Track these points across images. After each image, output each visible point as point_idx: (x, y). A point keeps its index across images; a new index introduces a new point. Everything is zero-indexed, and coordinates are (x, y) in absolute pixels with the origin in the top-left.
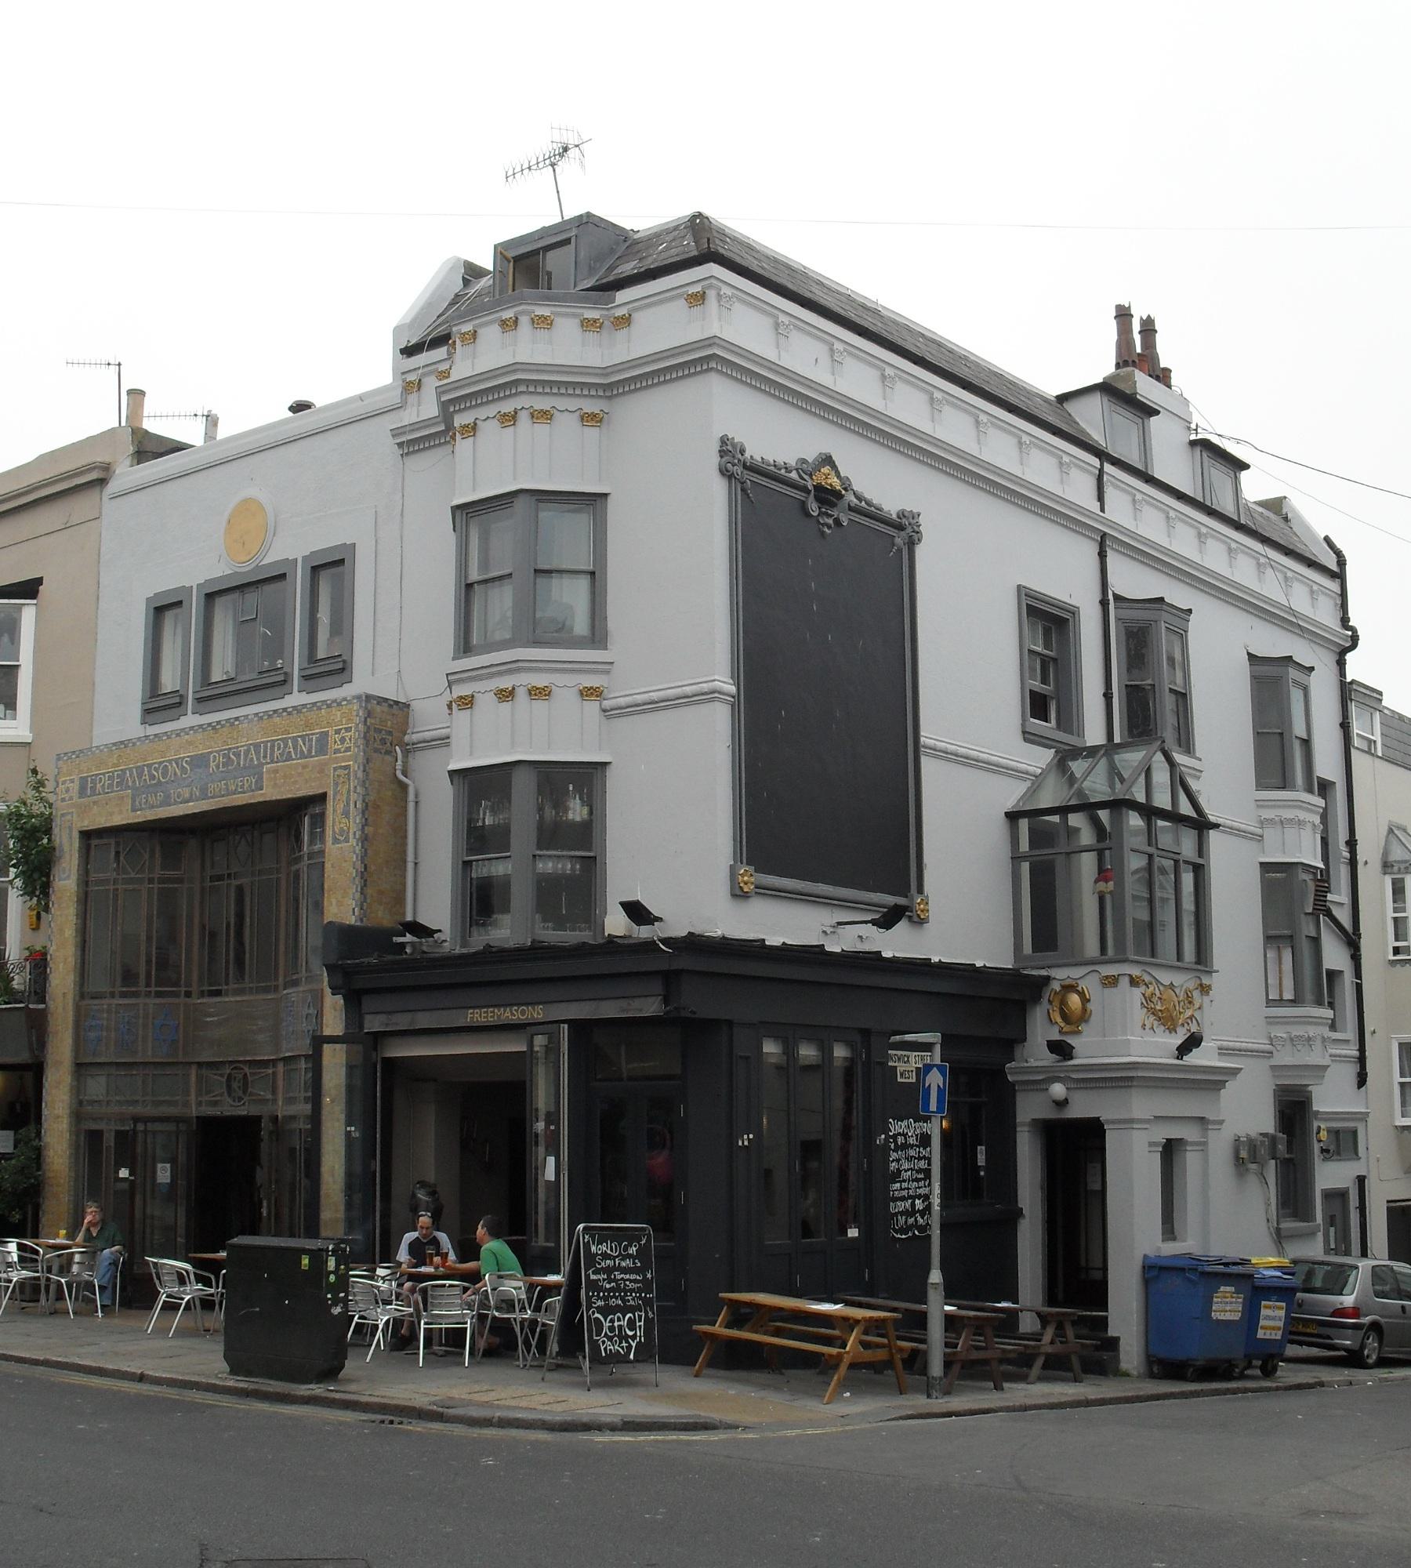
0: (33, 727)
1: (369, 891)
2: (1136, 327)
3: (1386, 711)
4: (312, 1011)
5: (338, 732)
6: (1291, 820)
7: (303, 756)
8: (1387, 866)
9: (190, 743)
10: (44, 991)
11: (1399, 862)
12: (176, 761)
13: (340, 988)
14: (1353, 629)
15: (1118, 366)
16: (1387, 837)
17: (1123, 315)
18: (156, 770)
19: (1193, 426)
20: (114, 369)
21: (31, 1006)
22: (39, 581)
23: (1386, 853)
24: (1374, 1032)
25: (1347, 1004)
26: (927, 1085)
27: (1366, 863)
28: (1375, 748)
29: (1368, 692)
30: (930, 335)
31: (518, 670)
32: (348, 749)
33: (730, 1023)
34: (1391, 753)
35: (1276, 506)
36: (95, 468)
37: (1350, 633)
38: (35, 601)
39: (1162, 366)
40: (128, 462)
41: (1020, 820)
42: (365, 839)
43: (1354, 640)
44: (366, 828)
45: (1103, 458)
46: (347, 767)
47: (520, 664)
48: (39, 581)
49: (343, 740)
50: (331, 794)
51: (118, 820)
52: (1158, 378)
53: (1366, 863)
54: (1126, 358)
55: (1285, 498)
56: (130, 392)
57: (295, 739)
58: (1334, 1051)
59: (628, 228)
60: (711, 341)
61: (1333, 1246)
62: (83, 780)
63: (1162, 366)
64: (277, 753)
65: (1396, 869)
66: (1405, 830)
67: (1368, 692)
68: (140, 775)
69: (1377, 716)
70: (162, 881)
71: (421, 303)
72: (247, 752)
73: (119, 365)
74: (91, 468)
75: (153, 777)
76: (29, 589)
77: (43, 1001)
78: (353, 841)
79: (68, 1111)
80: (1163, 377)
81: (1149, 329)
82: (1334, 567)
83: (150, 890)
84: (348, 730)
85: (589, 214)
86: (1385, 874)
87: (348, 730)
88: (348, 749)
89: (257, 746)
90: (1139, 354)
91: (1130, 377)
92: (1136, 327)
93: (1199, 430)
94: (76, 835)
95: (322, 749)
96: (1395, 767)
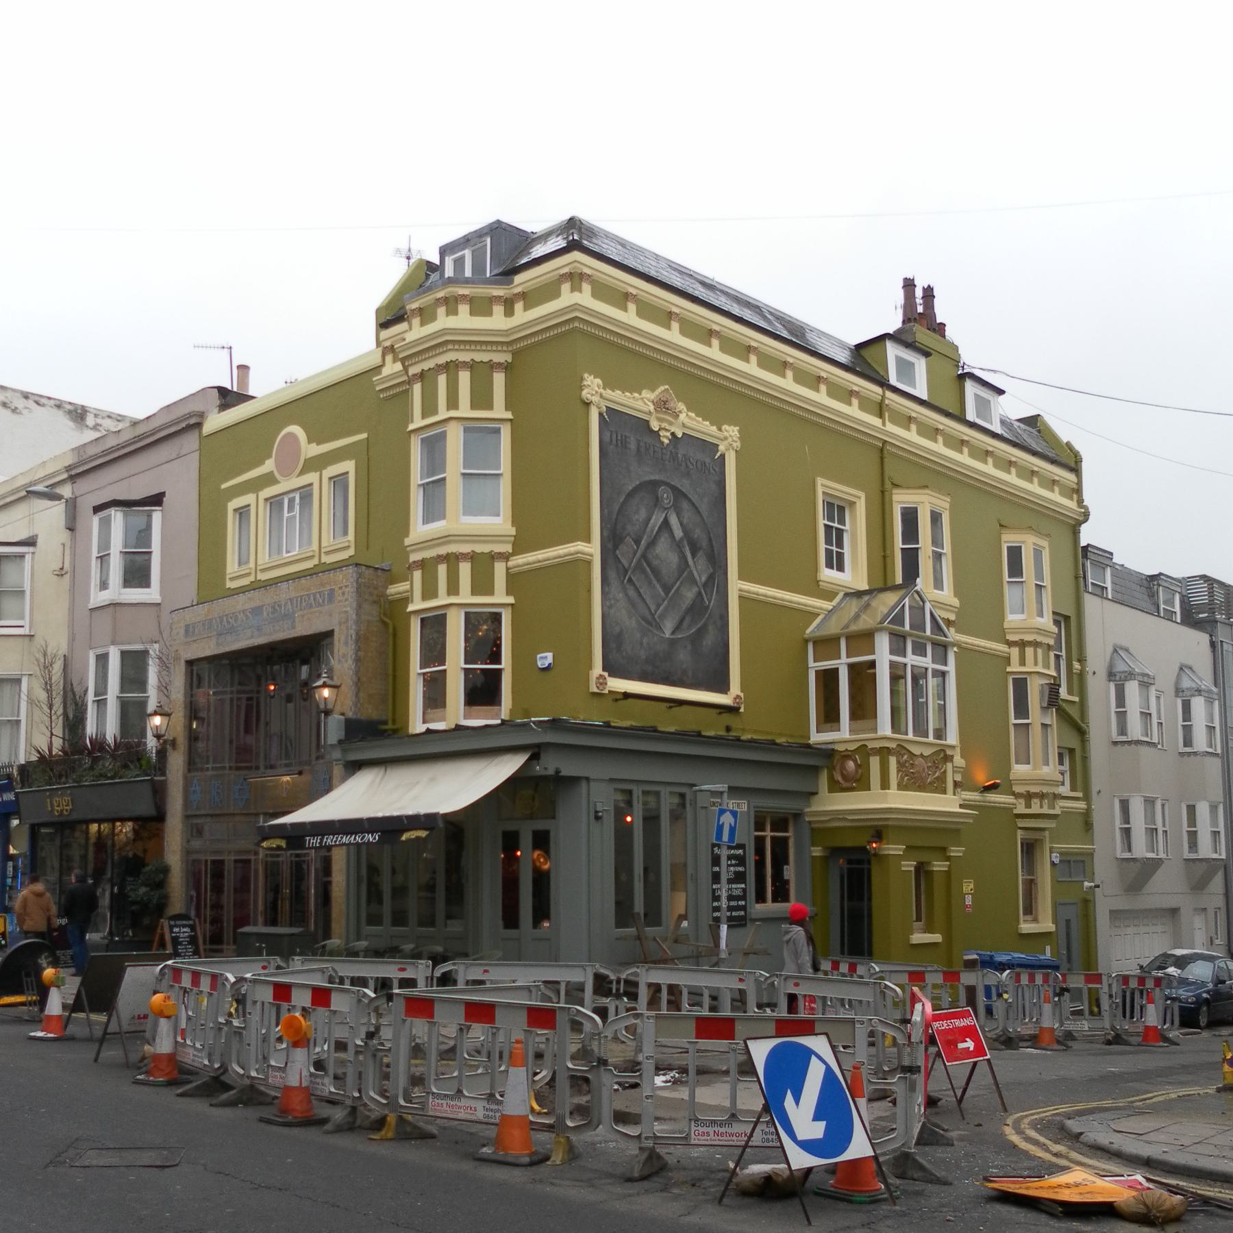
0: (162, 593)
1: (361, 694)
2: (919, 293)
3: (1117, 567)
4: (327, 777)
5: (341, 588)
6: (1031, 642)
7: (320, 605)
8: (1111, 675)
9: (250, 599)
10: (165, 767)
11: (1120, 672)
12: (243, 611)
13: (340, 760)
14: (1086, 508)
15: (904, 322)
16: (1113, 654)
17: (909, 285)
18: (231, 618)
19: (961, 364)
20: (226, 351)
21: (155, 778)
22: (163, 494)
23: (1111, 666)
24: (1099, 792)
25: (1078, 769)
26: (721, 823)
27: (1094, 673)
28: (1107, 593)
29: (1100, 553)
30: (733, 293)
31: (449, 542)
32: (346, 600)
33: (587, 779)
34: (1119, 596)
35: (1032, 421)
36: (195, 415)
37: (1083, 510)
38: (160, 508)
39: (938, 321)
40: (216, 410)
41: (414, 572)
42: (358, 660)
43: (1086, 516)
44: (359, 653)
45: (885, 388)
46: (346, 612)
47: (451, 538)
48: (163, 494)
49: (343, 594)
50: (336, 630)
51: (208, 653)
52: (934, 330)
53: (1094, 673)
54: (910, 316)
55: (1039, 415)
56: (239, 367)
57: (314, 595)
58: (1061, 804)
59: (529, 230)
60: (575, 307)
61: (10, 864)
62: (187, 626)
63: (938, 321)
64: (304, 604)
65: (1118, 678)
66: (1127, 650)
67: (1100, 553)
68: (222, 621)
69: (1108, 571)
70: (238, 692)
71: (394, 292)
72: (286, 603)
73: (231, 348)
74: (190, 415)
75: (228, 622)
76: (156, 500)
77: (164, 774)
78: (350, 662)
79: (180, 848)
80: (940, 329)
81: (929, 293)
82: (1073, 465)
83: (232, 700)
84: (346, 586)
85: (498, 222)
86: (1110, 681)
87: (346, 586)
88: (346, 600)
89: (291, 600)
90: (920, 313)
91: (911, 332)
92: (919, 293)
93: (965, 367)
94: (183, 663)
95: (331, 599)
96: (1123, 607)
